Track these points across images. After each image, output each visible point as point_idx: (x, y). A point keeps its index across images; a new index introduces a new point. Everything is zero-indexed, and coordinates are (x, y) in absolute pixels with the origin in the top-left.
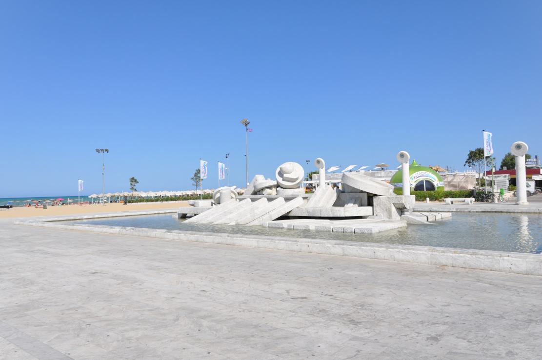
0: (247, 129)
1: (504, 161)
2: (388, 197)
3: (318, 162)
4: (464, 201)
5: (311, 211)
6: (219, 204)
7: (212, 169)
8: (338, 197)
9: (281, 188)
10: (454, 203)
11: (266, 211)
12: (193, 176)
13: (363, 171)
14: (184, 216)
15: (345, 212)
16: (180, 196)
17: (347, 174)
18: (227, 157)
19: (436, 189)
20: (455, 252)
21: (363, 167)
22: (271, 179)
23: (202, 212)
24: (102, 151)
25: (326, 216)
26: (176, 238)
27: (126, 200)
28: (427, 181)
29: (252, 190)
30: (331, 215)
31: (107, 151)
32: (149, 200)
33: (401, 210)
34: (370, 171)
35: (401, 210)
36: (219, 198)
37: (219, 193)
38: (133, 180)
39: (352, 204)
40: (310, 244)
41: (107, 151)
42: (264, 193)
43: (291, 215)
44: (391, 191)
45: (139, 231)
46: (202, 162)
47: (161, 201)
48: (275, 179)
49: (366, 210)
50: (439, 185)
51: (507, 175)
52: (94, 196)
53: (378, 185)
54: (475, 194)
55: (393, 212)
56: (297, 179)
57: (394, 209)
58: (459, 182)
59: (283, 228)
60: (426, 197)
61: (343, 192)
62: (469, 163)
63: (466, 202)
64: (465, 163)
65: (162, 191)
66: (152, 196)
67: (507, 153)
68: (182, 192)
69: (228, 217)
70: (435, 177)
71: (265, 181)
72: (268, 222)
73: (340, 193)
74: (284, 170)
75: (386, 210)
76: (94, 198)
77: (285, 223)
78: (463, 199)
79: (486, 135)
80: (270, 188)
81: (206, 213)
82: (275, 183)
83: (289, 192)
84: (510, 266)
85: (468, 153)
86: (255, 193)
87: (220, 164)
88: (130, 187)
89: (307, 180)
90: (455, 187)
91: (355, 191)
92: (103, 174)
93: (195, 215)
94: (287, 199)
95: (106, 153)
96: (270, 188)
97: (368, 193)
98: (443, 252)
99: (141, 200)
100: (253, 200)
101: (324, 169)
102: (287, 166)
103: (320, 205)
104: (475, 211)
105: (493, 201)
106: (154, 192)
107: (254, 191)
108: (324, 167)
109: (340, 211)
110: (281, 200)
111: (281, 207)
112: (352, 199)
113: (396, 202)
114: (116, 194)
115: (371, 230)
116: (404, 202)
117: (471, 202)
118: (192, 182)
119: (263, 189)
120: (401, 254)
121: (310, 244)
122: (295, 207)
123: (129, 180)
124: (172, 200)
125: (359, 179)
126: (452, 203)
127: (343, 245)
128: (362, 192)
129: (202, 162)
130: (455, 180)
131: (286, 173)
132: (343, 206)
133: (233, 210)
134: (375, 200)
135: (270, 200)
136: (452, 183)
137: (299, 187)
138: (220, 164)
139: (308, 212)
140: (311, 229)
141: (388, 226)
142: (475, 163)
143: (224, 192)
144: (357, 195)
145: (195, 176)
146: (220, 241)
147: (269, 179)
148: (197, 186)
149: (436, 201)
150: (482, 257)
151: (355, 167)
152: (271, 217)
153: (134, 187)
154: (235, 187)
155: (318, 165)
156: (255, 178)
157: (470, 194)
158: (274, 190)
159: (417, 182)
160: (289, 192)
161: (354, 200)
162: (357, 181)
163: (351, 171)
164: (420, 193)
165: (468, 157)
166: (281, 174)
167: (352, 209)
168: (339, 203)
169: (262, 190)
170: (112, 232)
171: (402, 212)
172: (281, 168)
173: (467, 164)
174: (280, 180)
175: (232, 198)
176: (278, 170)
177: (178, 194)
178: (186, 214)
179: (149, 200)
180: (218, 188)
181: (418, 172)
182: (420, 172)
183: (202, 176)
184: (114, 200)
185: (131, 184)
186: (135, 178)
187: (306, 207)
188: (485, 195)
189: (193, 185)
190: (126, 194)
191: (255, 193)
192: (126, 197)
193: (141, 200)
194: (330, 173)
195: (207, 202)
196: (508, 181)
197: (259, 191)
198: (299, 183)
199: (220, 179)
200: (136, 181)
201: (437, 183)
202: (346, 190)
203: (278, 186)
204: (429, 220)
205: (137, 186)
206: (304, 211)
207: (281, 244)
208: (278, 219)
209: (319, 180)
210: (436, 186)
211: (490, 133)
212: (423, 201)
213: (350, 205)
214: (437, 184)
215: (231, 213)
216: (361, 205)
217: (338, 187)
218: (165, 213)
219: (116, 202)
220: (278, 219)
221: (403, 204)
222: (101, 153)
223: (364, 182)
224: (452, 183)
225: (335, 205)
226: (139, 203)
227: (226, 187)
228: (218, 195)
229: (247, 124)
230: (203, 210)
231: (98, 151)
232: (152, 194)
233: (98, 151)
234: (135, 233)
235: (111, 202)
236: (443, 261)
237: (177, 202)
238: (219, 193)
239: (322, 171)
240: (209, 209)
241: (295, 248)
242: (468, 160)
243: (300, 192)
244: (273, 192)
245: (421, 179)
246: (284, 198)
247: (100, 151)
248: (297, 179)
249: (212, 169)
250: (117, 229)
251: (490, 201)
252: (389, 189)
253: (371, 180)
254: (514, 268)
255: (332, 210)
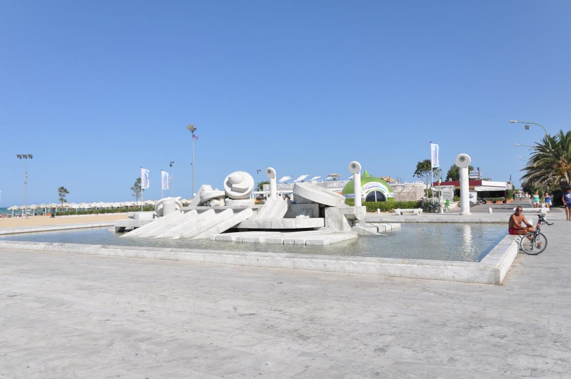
0: (194, 136)
1: (449, 172)
2: (340, 208)
3: (269, 171)
4: (413, 212)
5: (261, 223)
6: (162, 216)
7: (155, 178)
8: (289, 208)
9: (230, 198)
10: (403, 214)
11: (213, 223)
12: (133, 185)
13: (316, 181)
14: (122, 230)
15: (296, 223)
16: (89, 209)
17: (297, 184)
18: (171, 166)
19: (387, 200)
20: (403, 263)
21: (316, 178)
22: (219, 190)
23: (143, 225)
24: (25, 156)
25: (277, 228)
26: (112, 254)
27: (54, 213)
28: (379, 193)
29: (198, 201)
30: (282, 228)
31: (31, 157)
32: (81, 212)
33: (353, 221)
34: (323, 181)
35: (353, 221)
36: (162, 210)
37: (162, 205)
38: (63, 190)
39: (303, 216)
40: (259, 258)
41: (31, 157)
42: (211, 204)
43: (240, 227)
44: (343, 201)
45: (69, 247)
46: (143, 171)
47: (95, 213)
48: (223, 189)
49: (317, 222)
50: (390, 196)
51: (453, 186)
52: (15, 208)
53: (329, 196)
54: (423, 205)
55: (344, 223)
56: (246, 189)
57: (345, 221)
58: (408, 193)
59: (231, 241)
60: (377, 208)
61: (294, 203)
62: (418, 174)
63: (415, 212)
64: (414, 174)
65: (97, 202)
66: (86, 207)
67: (452, 165)
68: (120, 203)
69: (172, 230)
70: (386, 188)
71: (212, 191)
72: (215, 236)
73: (291, 204)
74: (232, 179)
75: (338, 221)
76: (15, 210)
77: (234, 236)
78: (412, 210)
79: (434, 147)
80: (217, 198)
81: (148, 226)
82: (223, 193)
83: (238, 204)
84: (453, 274)
85: (417, 164)
86: (201, 204)
87: (163, 173)
88: (59, 197)
89: (258, 191)
90: (404, 197)
91: (306, 202)
92: (25, 183)
93: (135, 228)
94: (236, 211)
95: (29, 159)
96: (217, 198)
97: (320, 204)
98: (392, 262)
99: (72, 212)
100: (199, 212)
101: (275, 179)
102: (236, 175)
103: (271, 216)
104: (422, 221)
105: (439, 212)
106: (88, 203)
107: (201, 201)
108: (275, 177)
109: (291, 223)
110: (229, 211)
111: (230, 219)
112: (303, 210)
113: (347, 213)
114: (42, 206)
115: (322, 242)
116: (355, 213)
117: (419, 212)
118: (132, 192)
119: (209, 200)
120: (351, 266)
121: (259, 258)
122: (244, 219)
123: (57, 190)
124: (108, 212)
125: (311, 190)
126: (402, 214)
127: (294, 257)
128: (313, 203)
129: (143, 171)
130: (405, 191)
131: (235, 183)
132: (295, 217)
133: (178, 222)
134: (327, 211)
135: (218, 211)
136: (401, 194)
137: (248, 198)
138: (163, 173)
139: (258, 224)
140: (260, 241)
141: (339, 238)
142: (423, 174)
143: (169, 203)
144: (309, 206)
145: (135, 185)
146: (162, 257)
147: (217, 189)
148: (138, 197)
149: (387, 212)
150: (427, 266)
151: (307, 177)
152: (218, 229)
153: (64, 198)
154: (180, 198)
155: (269, 175)
156: (201, 188)
157: (419, 205)
158: (222, 200)
159: (368, 193)
160: (238, 204)
161: (305, 211)
162: (308, 191)
163: (302, 181)
164: (371, 204)
165: (416, 169)
166: (229, 184)
167: (303, 221)
168: (290, 215)
169: (209, 201)
170: (36, 249)
171: (353, 223)
172: (229, 178)
173: (416, 175)
174: (228, 190)
175: (176, 209)
176: (227, 179)
177: (116, 205)
178: (125, 228)
179: (81, 212)
180: (161, 198)
181: (370, 183)
182: (372, 183)
183: (143, 185)
184: (39, 212)
185: (60, 195)
186: (65, 188)
187: (256, 219)
188: (433, 205)
189: (133, 195)
190: (54, 205)
191: (201, 204)
192: (54, 209)
193: (72, 212)
194: (282, 183)
195: (149, 214)
196: (453, 192)
197: (206, 202)
198: (248, 194)
199: (163, 189)
200: (65, 191)
201: (387, 194)
202: (298, 202)
203: (226, 196)
204: (379, 231)
205: (67, 197)
206: (254, 223)
207: (229, 258)
208: (223, 233)
209: (270, 190)
210: (386, 197)
211: (437, 145)
212: (374, 212)
213: (302, 216)
214: (388, 195)
215: (175, 226)
216: (312, 216)
217: (289, 198)
218: (100, 227)
219: (42, 214)
220: (223, 233)
221: (354, 215)
222: (23, 159)
223: (315, 193)
224: (401, 194)
225: (286, 216)
226: (69, 216)
227: (169, 198)
228: (161, 206)
229: (193, 130)
230: (144, 223)
231: (19, 156)
232: (86, 206)
233: (19, 156)
234: (63, 249)
235: (36, 214)
236: (392, 271)
237: (115, 214)
238: (162, 205)
239: (273, 181)
240: (151, 221)
241: (244, 262)
242: (417, 170)
243: (249, 203)
244: (221, 203)
245: (372, 189)
246: (233, 209)
247: (22, 157)
248: (246, 189)
249: (155, 178)
250: (42, 246)
251: (437, 211)
252: (340, 200)
253: (323, 191)
254: (457, 277)
255: (282, 222)
